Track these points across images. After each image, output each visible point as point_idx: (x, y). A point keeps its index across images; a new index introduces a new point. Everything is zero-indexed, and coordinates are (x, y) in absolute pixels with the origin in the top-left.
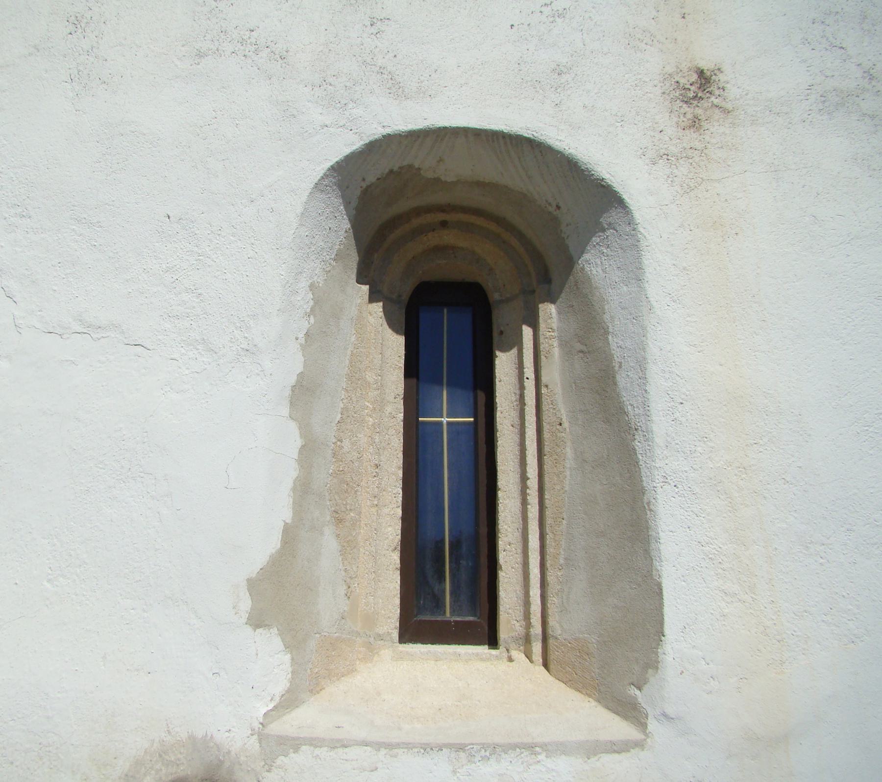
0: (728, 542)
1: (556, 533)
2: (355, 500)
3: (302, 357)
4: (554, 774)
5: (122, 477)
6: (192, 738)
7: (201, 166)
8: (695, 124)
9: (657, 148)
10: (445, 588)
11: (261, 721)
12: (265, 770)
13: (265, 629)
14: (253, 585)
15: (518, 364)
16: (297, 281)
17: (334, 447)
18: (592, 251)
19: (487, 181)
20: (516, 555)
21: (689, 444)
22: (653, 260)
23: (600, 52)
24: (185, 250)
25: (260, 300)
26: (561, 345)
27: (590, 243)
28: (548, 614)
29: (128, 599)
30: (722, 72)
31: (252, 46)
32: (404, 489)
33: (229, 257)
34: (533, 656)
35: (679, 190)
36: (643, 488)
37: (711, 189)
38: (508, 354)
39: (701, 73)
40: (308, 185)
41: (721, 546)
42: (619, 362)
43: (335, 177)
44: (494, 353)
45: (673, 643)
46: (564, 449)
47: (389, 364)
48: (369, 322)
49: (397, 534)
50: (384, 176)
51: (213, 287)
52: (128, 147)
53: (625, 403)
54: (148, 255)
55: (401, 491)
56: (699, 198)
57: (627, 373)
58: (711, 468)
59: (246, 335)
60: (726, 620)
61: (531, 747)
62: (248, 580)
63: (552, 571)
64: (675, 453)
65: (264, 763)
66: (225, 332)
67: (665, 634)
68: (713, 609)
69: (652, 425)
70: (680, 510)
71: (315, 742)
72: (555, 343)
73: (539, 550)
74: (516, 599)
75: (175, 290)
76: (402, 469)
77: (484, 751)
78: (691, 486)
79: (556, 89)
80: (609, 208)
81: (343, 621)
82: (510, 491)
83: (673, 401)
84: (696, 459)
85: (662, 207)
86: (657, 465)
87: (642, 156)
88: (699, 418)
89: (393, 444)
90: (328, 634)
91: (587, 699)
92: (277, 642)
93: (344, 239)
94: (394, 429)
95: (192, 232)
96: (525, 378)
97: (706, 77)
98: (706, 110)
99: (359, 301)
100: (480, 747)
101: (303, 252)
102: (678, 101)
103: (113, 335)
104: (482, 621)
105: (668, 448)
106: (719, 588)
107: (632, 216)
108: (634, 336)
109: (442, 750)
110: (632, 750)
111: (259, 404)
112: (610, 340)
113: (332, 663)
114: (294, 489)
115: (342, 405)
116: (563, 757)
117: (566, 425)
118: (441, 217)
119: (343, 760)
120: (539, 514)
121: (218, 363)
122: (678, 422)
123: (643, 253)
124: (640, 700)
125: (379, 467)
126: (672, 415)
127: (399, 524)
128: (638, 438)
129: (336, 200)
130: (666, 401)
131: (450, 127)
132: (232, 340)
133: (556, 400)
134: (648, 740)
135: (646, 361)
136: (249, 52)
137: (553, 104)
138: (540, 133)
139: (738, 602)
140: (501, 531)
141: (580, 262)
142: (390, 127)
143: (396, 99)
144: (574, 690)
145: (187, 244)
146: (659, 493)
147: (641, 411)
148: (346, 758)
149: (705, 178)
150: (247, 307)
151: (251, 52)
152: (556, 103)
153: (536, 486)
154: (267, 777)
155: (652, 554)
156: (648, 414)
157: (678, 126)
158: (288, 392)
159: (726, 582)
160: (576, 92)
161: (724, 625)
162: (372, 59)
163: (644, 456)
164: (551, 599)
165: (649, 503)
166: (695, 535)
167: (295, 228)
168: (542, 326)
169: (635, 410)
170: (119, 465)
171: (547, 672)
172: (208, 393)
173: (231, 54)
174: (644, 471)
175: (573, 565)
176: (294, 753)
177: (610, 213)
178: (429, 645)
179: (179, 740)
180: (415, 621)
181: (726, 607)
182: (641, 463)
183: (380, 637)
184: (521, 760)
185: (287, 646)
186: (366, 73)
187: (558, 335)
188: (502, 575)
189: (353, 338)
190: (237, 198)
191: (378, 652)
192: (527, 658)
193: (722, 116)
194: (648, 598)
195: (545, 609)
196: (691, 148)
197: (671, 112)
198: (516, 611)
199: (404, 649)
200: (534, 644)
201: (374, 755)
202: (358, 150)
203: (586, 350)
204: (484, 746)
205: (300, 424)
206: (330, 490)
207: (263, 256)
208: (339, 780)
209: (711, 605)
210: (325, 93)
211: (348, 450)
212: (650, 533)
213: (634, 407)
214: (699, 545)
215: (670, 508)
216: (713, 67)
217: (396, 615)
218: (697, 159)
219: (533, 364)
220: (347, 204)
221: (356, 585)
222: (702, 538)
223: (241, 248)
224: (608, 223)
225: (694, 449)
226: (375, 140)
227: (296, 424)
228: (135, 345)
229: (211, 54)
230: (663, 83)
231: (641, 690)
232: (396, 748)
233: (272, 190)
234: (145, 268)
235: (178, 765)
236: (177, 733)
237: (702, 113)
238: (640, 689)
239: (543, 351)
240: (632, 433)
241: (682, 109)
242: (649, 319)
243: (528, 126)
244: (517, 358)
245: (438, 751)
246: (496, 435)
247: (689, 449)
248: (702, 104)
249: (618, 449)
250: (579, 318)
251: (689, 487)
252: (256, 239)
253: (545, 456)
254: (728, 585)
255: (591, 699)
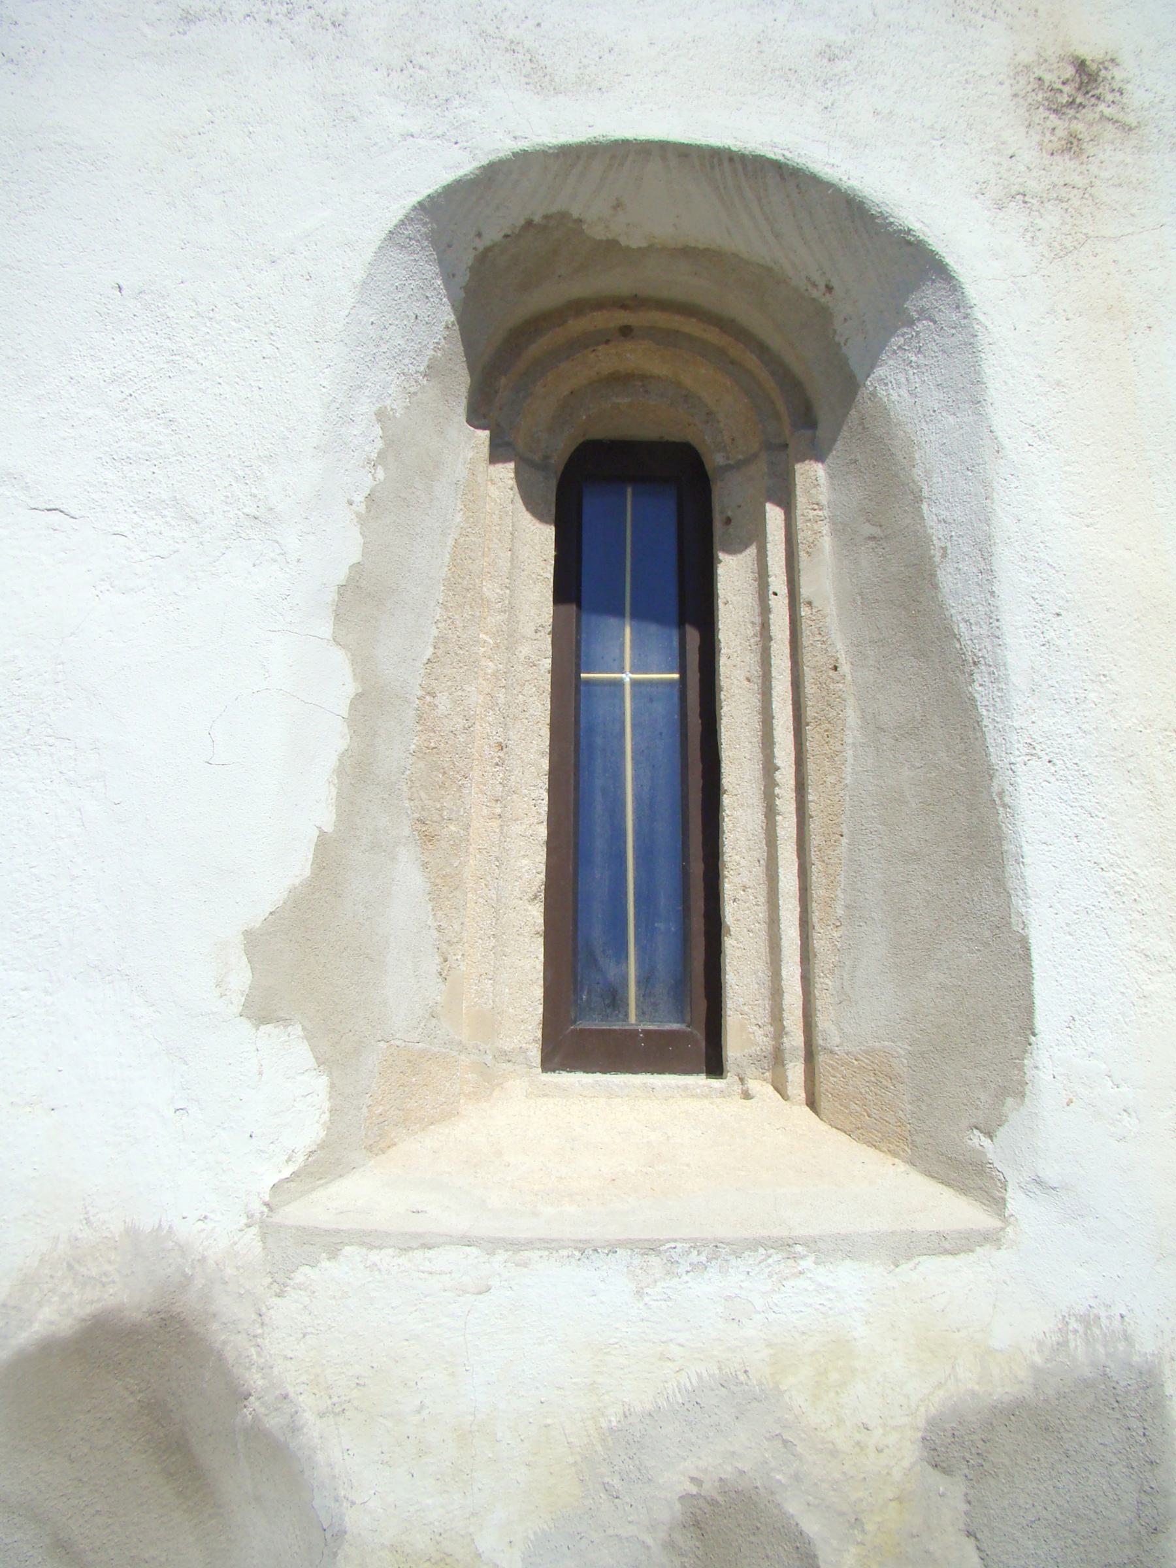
0: (1149, 864)
1: (828, 861)
2: (459, 802)
3: (361, 537)
4: (831, 1295)
5: (14, 745)
6: (132, 1232)
7: (183, 203)
8: (1072, 145)
9: (1006, 183)
10: (627, 973)
11: (267, 1199)
12: (274, 1294)
13: (278, 1027)
14: (254, 942)
15: (759, 574)
16: (353, 400)
17: (420, 705)
18: (891, 362)
19: (701, 246)
20: (756, 907)
21: (1074, 687)
22: (1001, 367)
23: (902, 27)
24: (147, 345)
25: (282, 429)
26: (835, 532)
27: (887, 348)
28: (816, 1009)
29: (16, 969)
30: (1118, 65)
31: (282, 5)
32: (551, 791)
33: (227, 357)
34: (789, 1088)
35: (1046, 253)
36: (990, 767)
37: (1102, 253)
38: (740, 556)
39: (1081, 66)
40: (376, 233)
41: (1137, 870)
42: (942, 548)
43: (425, 224)
44: (715, 556)
45: (1051, 1047)
46: (842, 711)
47: (526, 573)
48: (490, 496)
49: (539, 870)
50: (517, 231)
51: (195, 408)
52: (51, 169)
53: (954, 619)
54: (78, 353)
55: (545, 795)
56: (1082, 266)
57: (956, 565)
58: (1115, 729)
59: (255, 491)
60: (1149, 1005)
61: (786, 1246)
62: (247, 934)
63: (822, 931)
64: (1049, 703)
65: (270, 1280)
66: (216, 486)
67: (1036, 1031)
68: (1124, 985)
69: (1006, 653)
70: (1059, 804)
71: (368, 1239)
72: (825, 529)
73: (798, 894)
74: (757, 986)
75: (126, 414)
76: (548, 755)
77: (696, 1253)
78: (1078, 762)
79: (826, 84)
80: (921, 283)
81: (434, 1021)
82: (745, 794)
83: (1042, 610)
84: (1086, 713)
85: (1016, 280)
86: (1015, 724)
87: (979, 196)
88: (1090, 641)
89: (531, 711)
90: (404, 1044)
91: (890, 1159)
92: (302, 1053)
93: (443, 340)
94: (535, 686)
95: (161, 315)
96: (771, 592)
97: (1091, 73)
98: (1091, 125)
99: (470, 454)
100: (688, 1245)
101: (364, 350)
102: (1041, 109)
103: (8, 494)
104: (695, 1032)
105: (1036, 693)
106: (1135, 946)
107: (963, 293)
108: (969, 500)
109: (616, 1252)
110: (978, 1248)
111: (274, 612)
112: (924, 511)
113: (411, 1099)
114: (340, 771)
115: (435, 632)
116: (848, 1262)
117: (845, 668)
118: (624, 318)
119: (423, 1272)
120: (797, 831)
121: (201, 540)
122: (1053, 648)
123: (982, 355)
124: (990, 1156)
125: (505, 750)
126: (1042, 635)
127: (542, 853)
128: (980, 678)
129: (428, 267)
130: (1030, 611)
131: (635, 140)
132: (228, 500)
133: (826, 627)
134: (1008, 1229)
135: (992, 541)
136: (277, 14)
137: (820, 108)
138: (796, 153)
139: (1170, 973)
140: (729, 865)
141: (869, 384)
142: (526, 138)
143: (538, 93)
144: (865, 1146)
145: (151, 335)
146: (1020, 774)
147: (985, 630)
148: (430, 1270)
149: (1091, 234)
150: (257, 442)
151: (280, 16)
152: (826, 106)
153: (792, 782)
154: (275, 1308)
155: (1010, 885)
156: (998, 633)
157: (1041, 149)
158: (331, 596)
159: (1147, 936)
160: (861, 89)
161: (1146, 1013)
162: (497, 28)
163: (991, 709)
164: (822, 980)
165: (1001, 794)
166: (1089, 850)
167: (350, 307)
168: (801, 500)
169: (973, 628)
170: (9, 724)
171: (814, 1114)
172: (180, 593)
173: (245, 18)
174: (991, 736)
175: (860, 917)
176: (329, 1259)
177: (923, 291)
178: (598, 1074)
179: (106, 1237)
180: (573, 1031)
181: (1148, 982)
182: (985, 723)
183: (505, 1056)
184: (767, 1270)
185: (321, 1061)
186: (485, 50)
187: (830, 514)
188: (730, 944)
189: (459, 517)
190: (246, 255)
191: (502, 1084)
192: (778, 1092)
193: (1119, 135)
194: (1003, 968)
195: (810, 1001)
196: (1065, 185)
197: (1030, 125)
198: (756, 1008)
199: (550, 1079)
200: (790, 1065)
201: (484, 1263)
202: (469, 177)
203: (882, 535)
204: (696, 1244)
205: (352, 655)
206: (411, 781)
207: (291, 353)
208: (416, 1311)
209: (1120, 978)
210: (411, 81)
211: (446, 713)
212: (1005, 848)
213: (971, 624)
214: (1097, 868)
215: (1041, 802)
216: (1101, 56)
217: (536, 1017)
218: (1076, 202)
219: (784, 570)
220: (449, 277)
221: (459, 957)
222: (1101, 856)
223: (251, 340)
224: (919, 309)
225: (1083, 695)
226: (499, 161)
227: (346, 654)
228: (48, 510)
229: (208, 16)
230: (1015, 79)
231: (994, 1138)
232: (526, 1250)
233: (310, 243)
234: (72, 375)
235: (104, 1285)
236: (104, 1223)
237: (1084, 130)
238: (990, 1135)
239: (802, 543)
240: (967, 669)
241: (1048, 123)
242: (996, 467)
243: (775, 140)
244: (755, 562)
245: (608, 1255)
246: (720, 697)
247: (1073, 695)
248: (1084, 114)
249: (943, 701)
250: (868, 480)
251: (1076, 764)
252: (277, 325)
253: (808, 725)
254: (1151, 940)
255: (897, 1161)
